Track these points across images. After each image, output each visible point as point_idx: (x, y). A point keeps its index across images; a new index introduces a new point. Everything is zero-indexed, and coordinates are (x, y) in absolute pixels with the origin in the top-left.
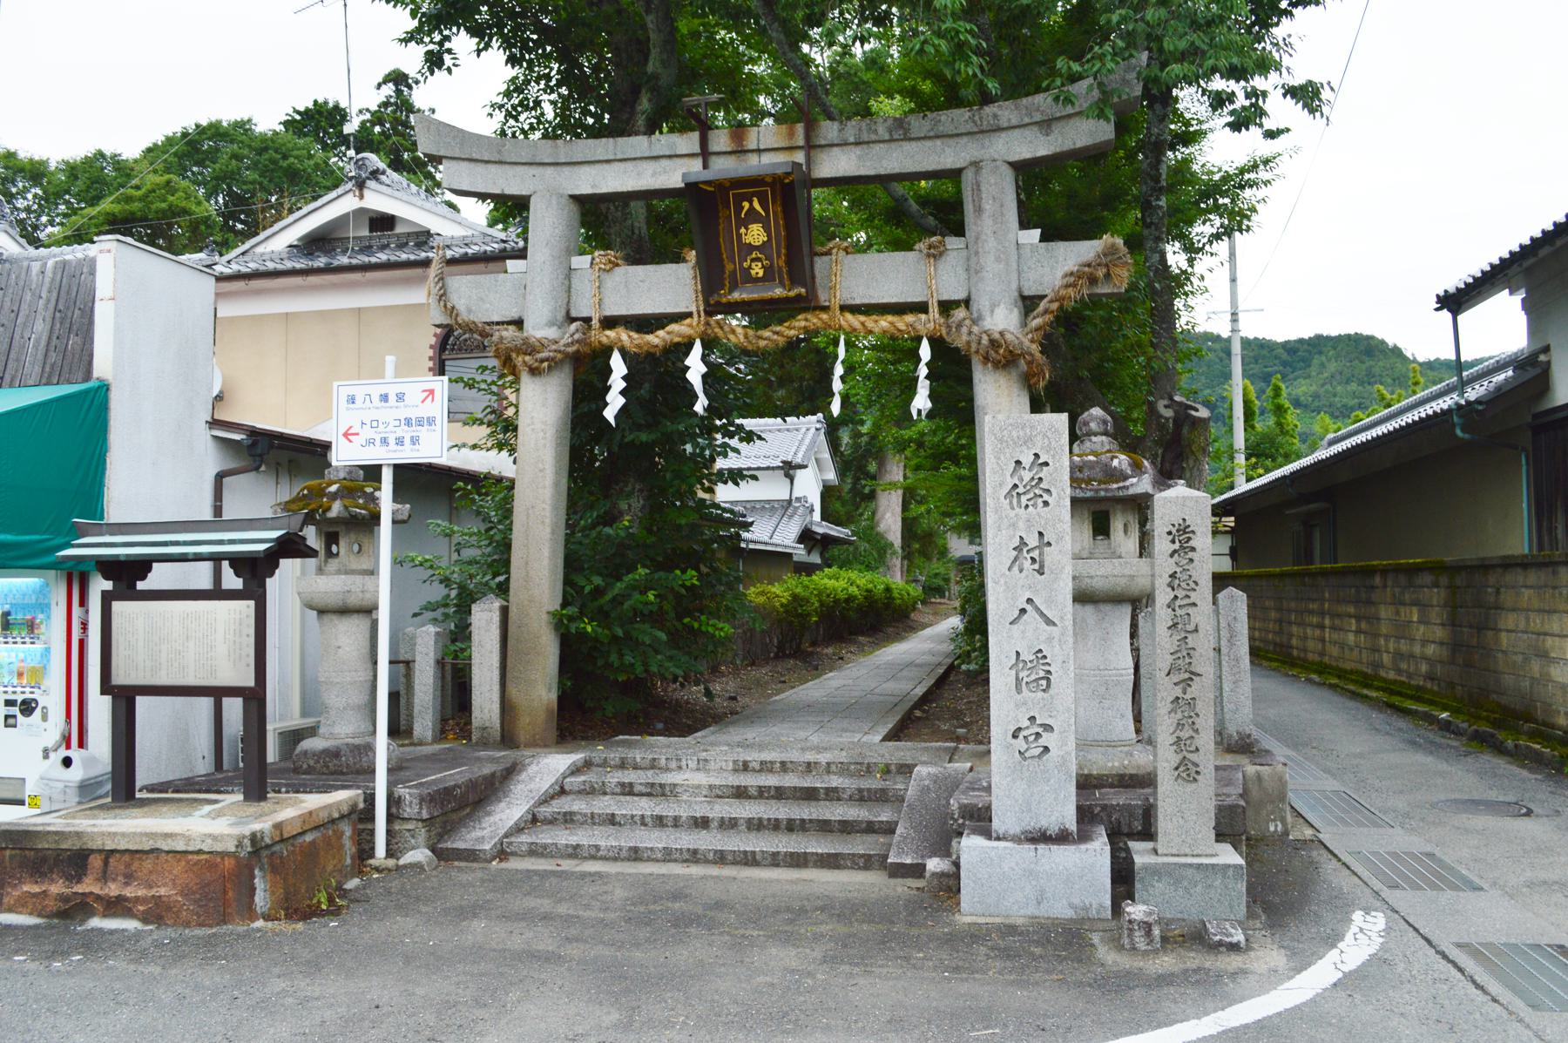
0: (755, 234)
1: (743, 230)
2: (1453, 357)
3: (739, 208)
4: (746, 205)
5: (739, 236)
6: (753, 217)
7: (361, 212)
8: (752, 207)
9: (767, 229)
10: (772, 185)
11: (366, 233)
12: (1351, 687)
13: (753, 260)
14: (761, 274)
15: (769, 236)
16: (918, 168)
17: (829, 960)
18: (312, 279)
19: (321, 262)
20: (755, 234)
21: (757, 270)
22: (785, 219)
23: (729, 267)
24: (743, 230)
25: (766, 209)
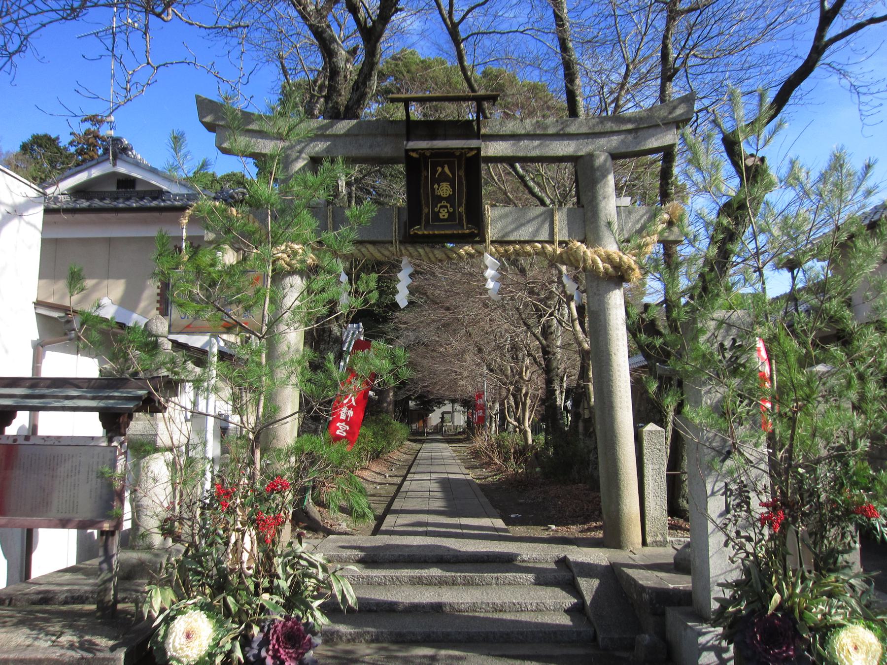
0: (445, 190)
1: (436, 186)
2: (404, 118)
3: (434, 171)
4: (440, 169)
5: (433, 190)
6: (444, 178)
7: (115, 174)
8: (443, 172)
9: (453, 186)
10: (459, 158)
11: (114, 189)
12: (642, 221)
13: (441, 207)
14: (446, 216)
15: (454, 191)
16: (812, 34)
17: (518, 555)
18: (78, 216)
19: (85, 204)
20: (445, 190)
21: (444, 214)
22: (467, 180)
23: (425, 210)
24: (436, 186)
25: (453, 174)
